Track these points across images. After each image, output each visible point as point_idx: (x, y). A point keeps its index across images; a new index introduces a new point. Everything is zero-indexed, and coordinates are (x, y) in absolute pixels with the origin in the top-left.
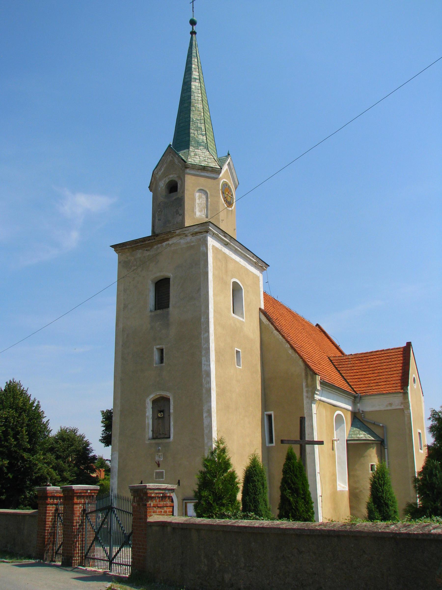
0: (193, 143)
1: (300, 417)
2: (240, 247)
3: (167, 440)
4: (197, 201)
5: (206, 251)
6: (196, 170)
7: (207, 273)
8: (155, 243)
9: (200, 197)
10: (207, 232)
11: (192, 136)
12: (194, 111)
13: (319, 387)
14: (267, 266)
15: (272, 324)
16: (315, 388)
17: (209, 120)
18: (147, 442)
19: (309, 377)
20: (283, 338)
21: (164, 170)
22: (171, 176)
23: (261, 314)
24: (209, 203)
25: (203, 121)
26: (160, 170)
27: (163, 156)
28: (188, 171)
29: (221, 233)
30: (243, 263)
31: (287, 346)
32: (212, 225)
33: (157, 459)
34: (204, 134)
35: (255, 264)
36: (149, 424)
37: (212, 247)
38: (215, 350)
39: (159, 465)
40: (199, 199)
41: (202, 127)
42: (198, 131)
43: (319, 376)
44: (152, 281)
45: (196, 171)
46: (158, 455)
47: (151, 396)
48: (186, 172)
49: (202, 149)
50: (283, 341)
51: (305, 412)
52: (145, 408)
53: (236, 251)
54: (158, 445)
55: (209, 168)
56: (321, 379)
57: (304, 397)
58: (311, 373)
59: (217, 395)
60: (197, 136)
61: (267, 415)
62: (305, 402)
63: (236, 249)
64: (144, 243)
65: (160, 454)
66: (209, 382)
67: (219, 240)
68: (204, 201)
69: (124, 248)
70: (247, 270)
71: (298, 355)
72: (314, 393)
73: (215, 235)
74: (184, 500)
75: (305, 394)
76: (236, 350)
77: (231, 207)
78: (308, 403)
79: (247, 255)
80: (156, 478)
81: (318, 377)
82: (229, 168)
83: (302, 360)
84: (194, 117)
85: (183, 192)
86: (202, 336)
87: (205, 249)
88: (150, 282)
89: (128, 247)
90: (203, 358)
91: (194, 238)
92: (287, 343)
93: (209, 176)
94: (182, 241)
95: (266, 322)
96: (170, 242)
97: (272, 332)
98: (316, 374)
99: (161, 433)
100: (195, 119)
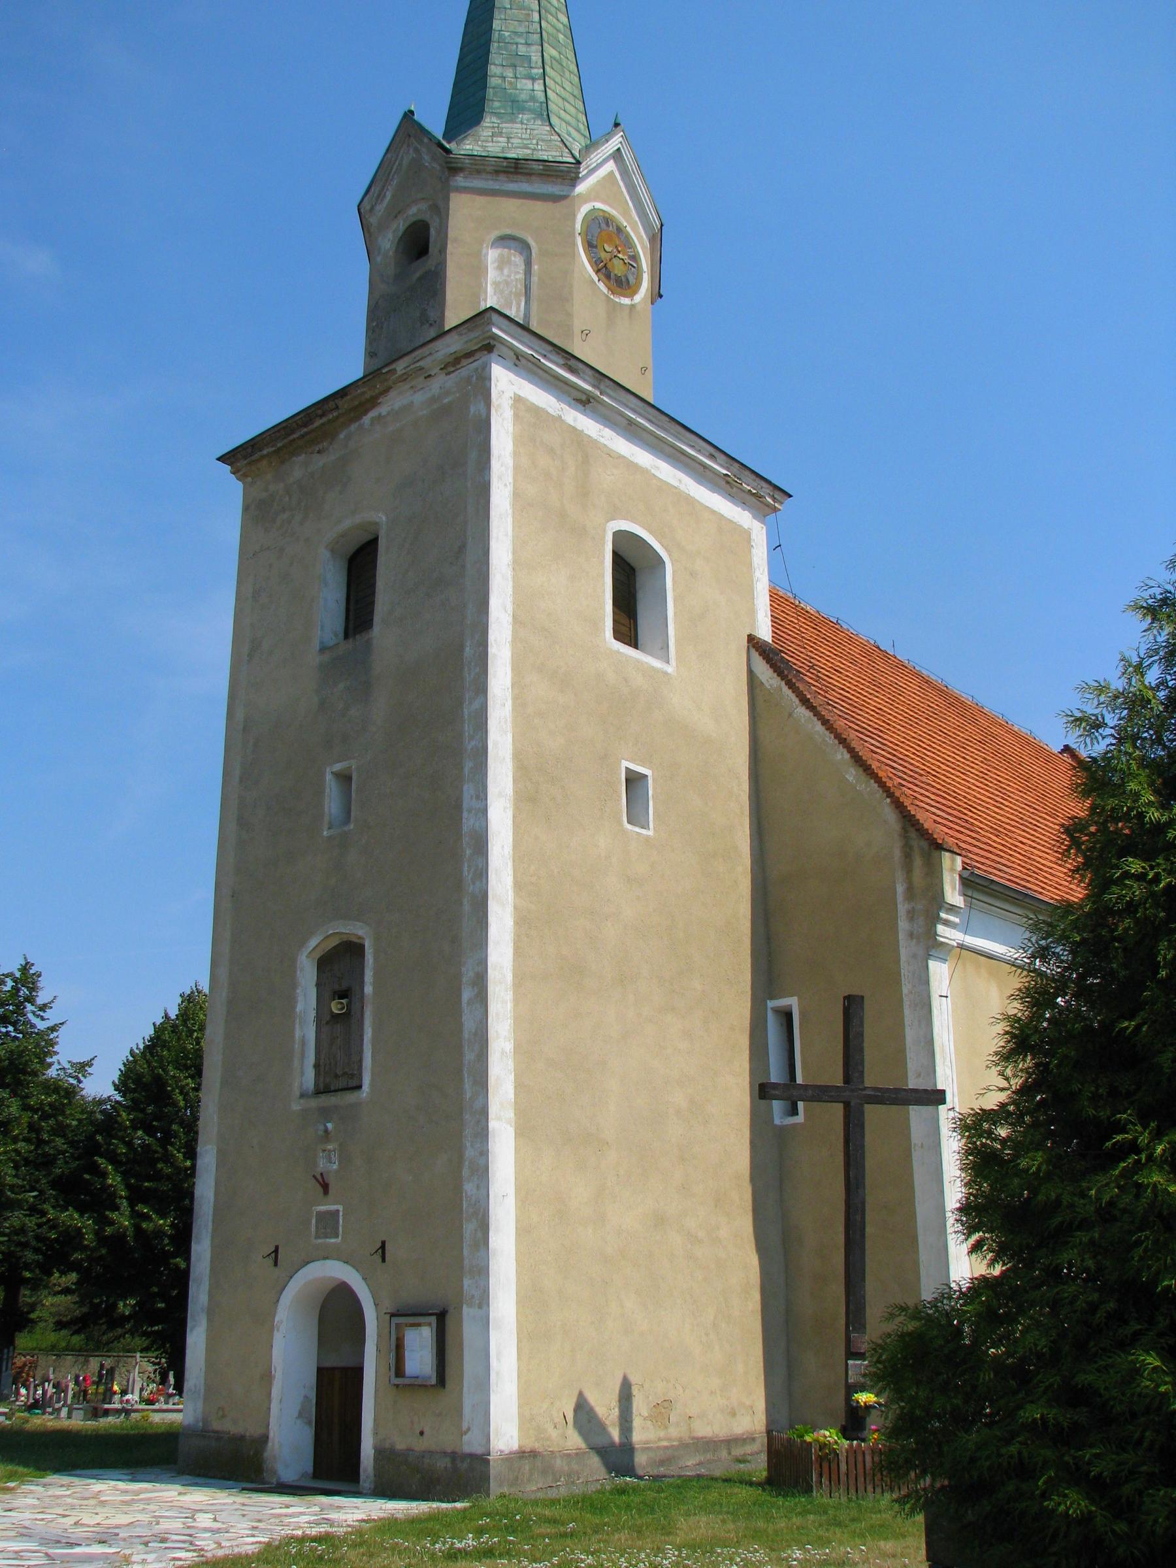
0: (497, 104)
1: (845, 998)
2: (647, 415)
3: (350, 1098)
4: (492, 274)
5: (484, 416)
6: (489, 177)
7: (484, 490)
8: (341, 420)
9: (502, 263)
10: (489, 348)
11: (493, 85)
12: (505, 8)
13: (953, 895)
14: (778, 495)
15: (790, 685)
16: (936, 901)
17: (561, 37)
18: (296, 1107)
19: (918, 862)
20: (827, 729)
21: (393, 196)
22: (413, 210)
23: (755, 655)
24: (535, 279)
25: (537, 37)
26: (380, 197)
27: (388, 150)
28: (460, 180)
29: (549, 355)
30: (665, 471)
31: (843, 755)
32: (506, 322)
33: (322, 1165)
34: (537, 74)
35: (728, 482)
36: (303, 1043)
37: (511, 402)
38: (518, 756)
39: (325, 1187)
40: (500, 268)
41: (533, 54)
42: (516, 66)
43: (959, 859)
44: (332, 551)
45: (487, 180)
46: (324, 1151)
47: (313, 943)
48: (451, 183)
49: (528, 120)
50: (827, 739)
51: (905, 991)
52: (294, 985)
53: (630, 430)
54: (325, 1113)
55: (535, 166)
56: (964, 868)
57: (901, 936)
58: (924, 844)
59: (522, 921)
60: (511, 83)
61: (777, 1011)
62: (904, 953)
63: (631, 422)
64: (310, 427)
65: (330, 1147)
66: (481, 874)
67: (547, 382)
68: (519, 273)
69: (256, 456)
70: (690, 500)
71: (876, 785)
72: (934, 919)
73: (523, 361)
74: (393, 1315)
75: (903, 925)
76: (626, 768)
77: (631, 296)
78: (914, 956)
79: (647, 425)
80: (317, 1237)
81: (953, 861)
82: (618, 170)
83: (892, 802)
84: (506, 27)
85: (443, 250)
86: (466, 711)
87: (482, 406)
88: (324, 554)
89: (265, 452)
90: (465, 787)
91: (451, 381)
92: (841, 746)
93: (538, 191)
94: (419, 398)
95: (771, 682)
96: (383, 409)
97: (790, 715)
98: (940, 847)
99: (339, 1072)
100: (507, 34)
